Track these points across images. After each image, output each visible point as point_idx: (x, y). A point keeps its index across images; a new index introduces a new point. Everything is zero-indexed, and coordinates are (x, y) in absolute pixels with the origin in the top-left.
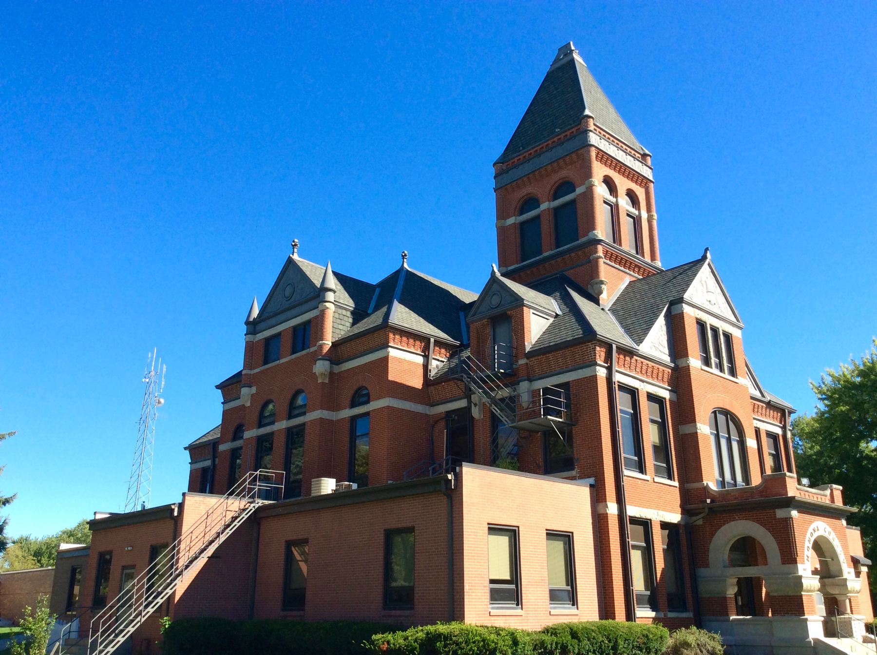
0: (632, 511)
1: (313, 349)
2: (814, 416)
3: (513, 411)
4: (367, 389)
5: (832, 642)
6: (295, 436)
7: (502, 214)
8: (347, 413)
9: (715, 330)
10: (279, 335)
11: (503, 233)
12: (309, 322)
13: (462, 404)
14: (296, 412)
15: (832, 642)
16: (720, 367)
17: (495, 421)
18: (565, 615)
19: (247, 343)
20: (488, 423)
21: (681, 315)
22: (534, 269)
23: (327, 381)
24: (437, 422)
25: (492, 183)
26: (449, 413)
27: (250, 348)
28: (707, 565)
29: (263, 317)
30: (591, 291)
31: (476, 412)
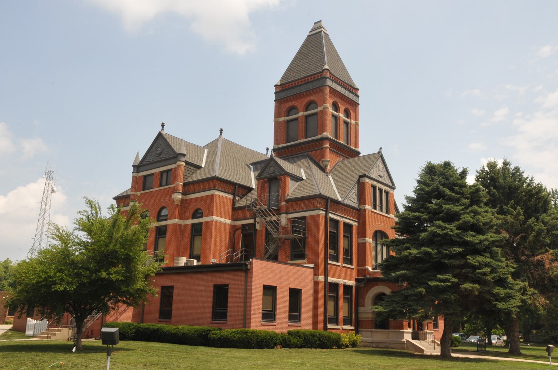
0: (330, 279)
1: (172, 186)
2: (536, 182)
3: (277, 229)
4: (201, 210)
5: (415, 342)
6: (161, 232)
7: (278, 114)
8: (190, 222)
9: (381, 190)
10: (152, 174)
11: (277, 125)
12: (170, 170)
13: (251, 221)
14: (161, 218)
15: (415, 342)
16: (381, 210)
17: (268, 233)
18: (295, 327)
19: (133, 177)
20: (264, 232)
21: (364, 184)
22: (293, 149)
23: (180, 204)
24: (237, 230)
25: (273, 97)
26: (244, 226)
27: (135, 180)
28: (363, 306)
29: (143, 164)
30: (321, 164)
31: (258, 227)
